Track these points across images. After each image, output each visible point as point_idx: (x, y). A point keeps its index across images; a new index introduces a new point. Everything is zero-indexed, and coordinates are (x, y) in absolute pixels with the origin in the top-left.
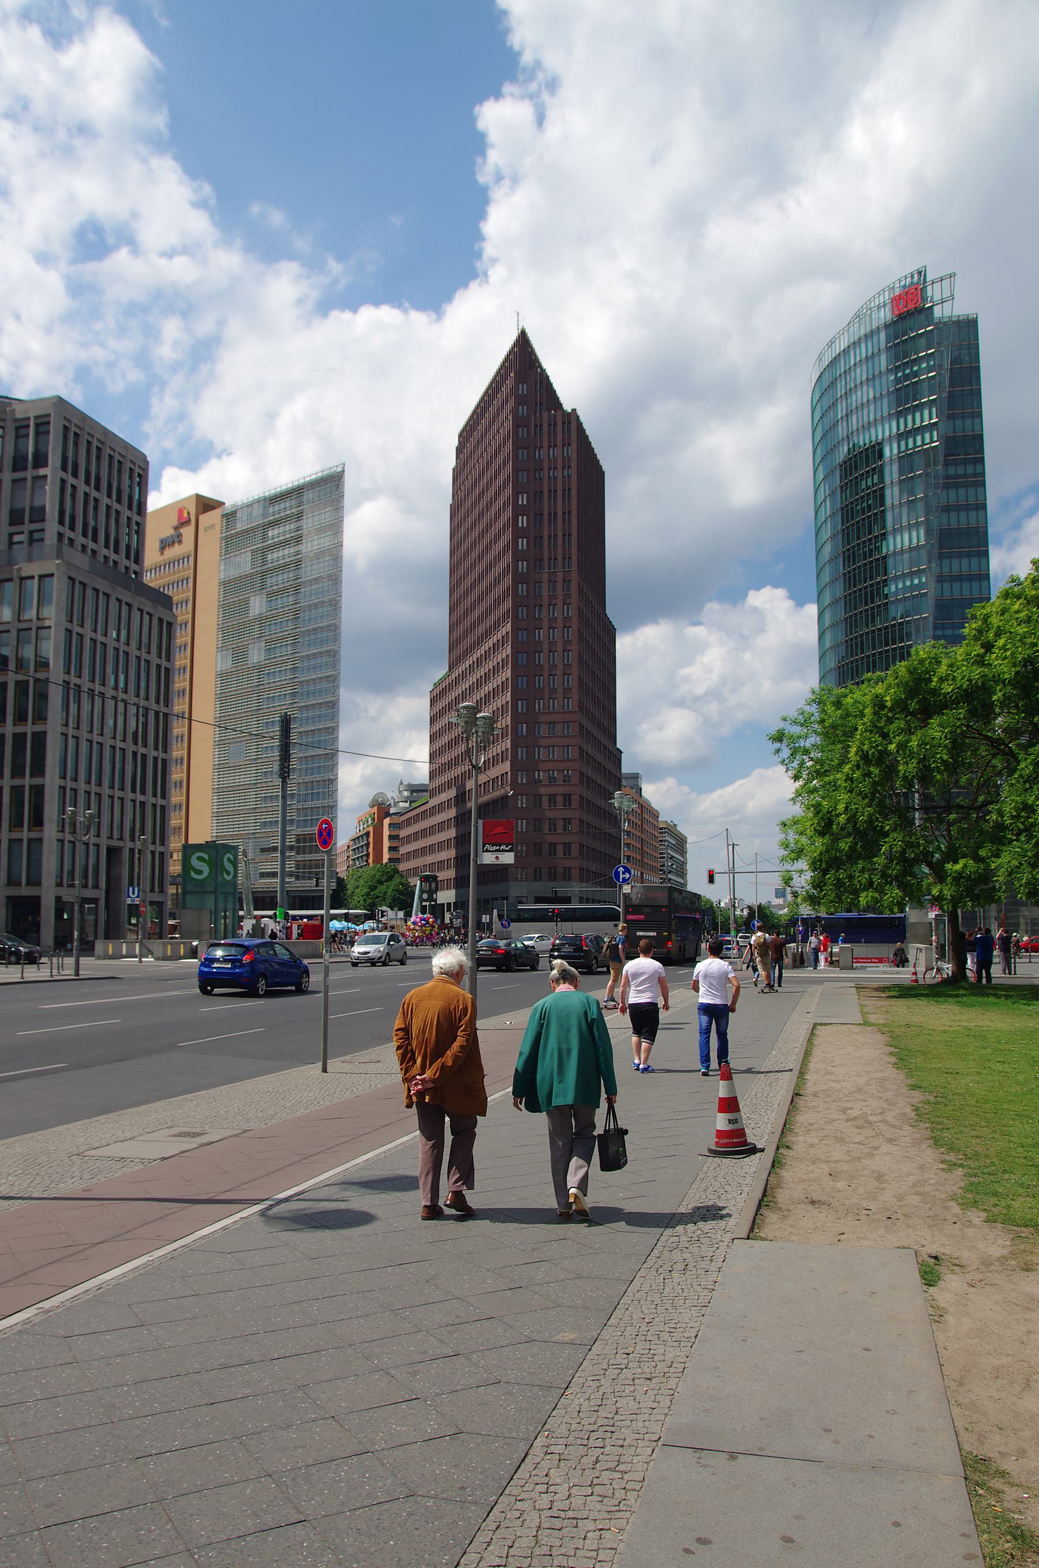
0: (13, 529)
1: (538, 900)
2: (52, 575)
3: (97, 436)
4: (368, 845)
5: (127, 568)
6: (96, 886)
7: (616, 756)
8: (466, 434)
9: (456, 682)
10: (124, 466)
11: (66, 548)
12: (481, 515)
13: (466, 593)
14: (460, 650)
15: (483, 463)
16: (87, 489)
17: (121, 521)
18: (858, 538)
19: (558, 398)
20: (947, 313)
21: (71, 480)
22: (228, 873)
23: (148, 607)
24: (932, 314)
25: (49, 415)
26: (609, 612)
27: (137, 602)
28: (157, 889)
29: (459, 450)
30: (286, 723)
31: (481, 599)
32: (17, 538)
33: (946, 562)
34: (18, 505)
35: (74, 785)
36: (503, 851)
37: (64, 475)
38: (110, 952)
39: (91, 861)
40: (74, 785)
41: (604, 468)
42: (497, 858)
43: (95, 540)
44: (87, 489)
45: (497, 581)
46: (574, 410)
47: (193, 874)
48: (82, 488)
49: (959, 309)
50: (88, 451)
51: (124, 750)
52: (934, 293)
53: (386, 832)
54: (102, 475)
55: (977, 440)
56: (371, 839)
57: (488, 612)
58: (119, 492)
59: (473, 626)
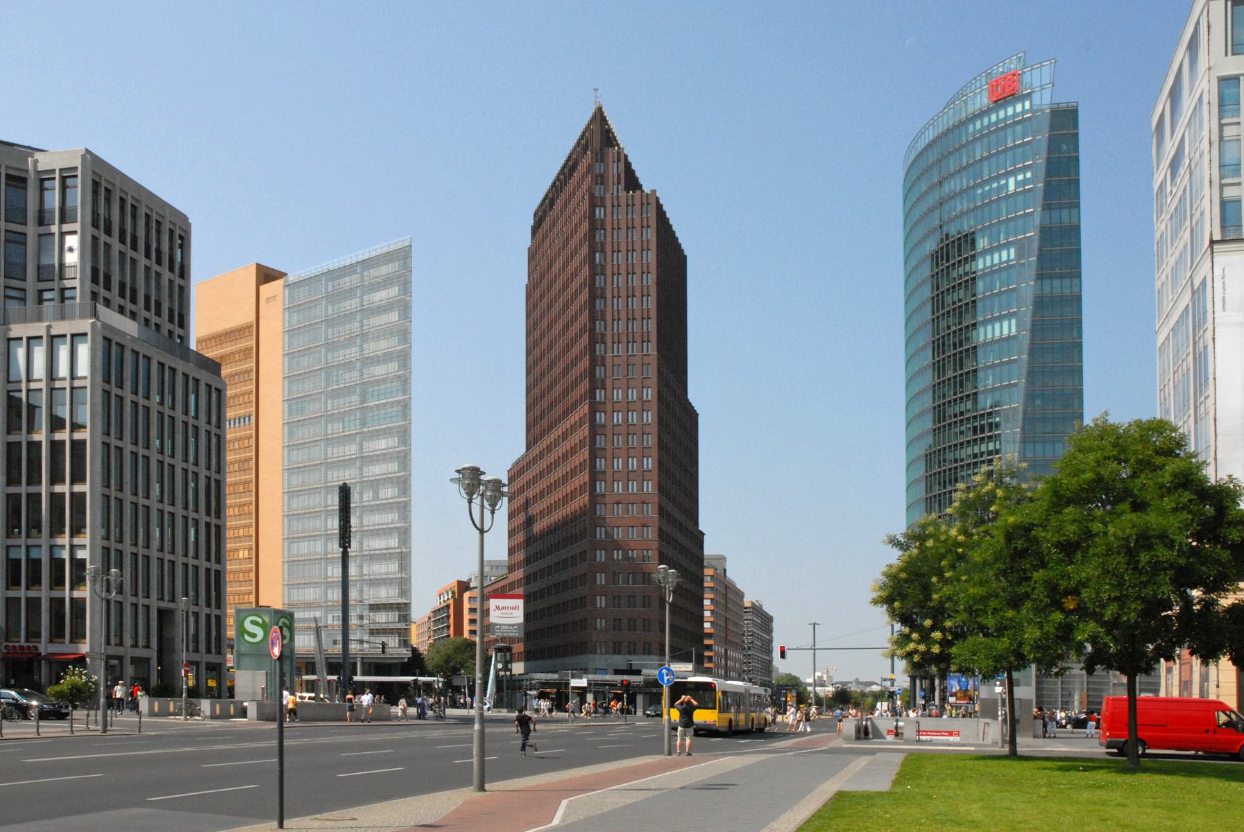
0: (42, 286)
1: (617, 672)
4: (448, 617)
5: (170, 332)
6: (148, 646)
7: (698, 538)
9: (535, 461)
10: (163, 227)
11: (101, 308)
15: (558, 243)
18: (955, 394)
19: (680, 245)
23: (194, 372)
25: (76, 168)
26: (692, 397)
27: (181, 366)
28: (213, 650)
30: (345, 492)
32: (47, 295)
33: (1047, 283)
35: (171, 557)
37: (96, 232)
38: (156, 709)
39: (192, 631)
40: (171, 557)
41: (686, 253)
46: (654, 192)
47: (247, 637)
48: (116, 246)
50: (147, 225)
53: (466, 606)
54: (138, 234)
55: (1074, 231)
56: (451, 611)
58: (159, 252)
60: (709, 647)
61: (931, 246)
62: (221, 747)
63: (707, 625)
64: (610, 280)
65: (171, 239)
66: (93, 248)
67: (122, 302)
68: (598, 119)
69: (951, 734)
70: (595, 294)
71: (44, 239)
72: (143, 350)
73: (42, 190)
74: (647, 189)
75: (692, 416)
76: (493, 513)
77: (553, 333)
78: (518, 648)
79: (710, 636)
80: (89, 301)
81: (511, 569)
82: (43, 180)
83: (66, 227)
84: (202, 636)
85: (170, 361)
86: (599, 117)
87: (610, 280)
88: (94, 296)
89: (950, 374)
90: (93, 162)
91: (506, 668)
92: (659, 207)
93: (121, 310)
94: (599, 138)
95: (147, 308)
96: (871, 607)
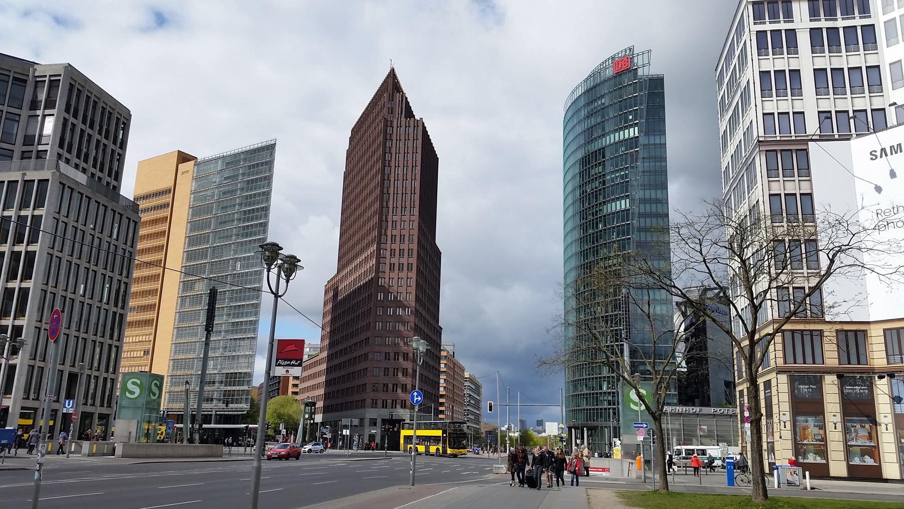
2: (48, 180)
3: (95, 93)
5: (108, 183)
8: (355, 131)
11: (62, 164)
12: (362, 179)
13: (351, 226)
14: (344, 260)
16: (99, 137)
17: (107, 150)
20: (646, 73)
21: (72, 120)
22: (154, 394)
24: (637, 73)
26: (438, 242)
28: (105, 405)
29: (351, 139)
31: (359, 229)
34: (30, 133)
36: (293, 365)
37: (67, 116)
42: (287, 371)
43: (101, 170)
44: (99, 137)
45: (369, 219)
46: (421, 119)
48: (80, 126)
49: (653, 70)
51: (91, 305)
52: (639, 61)
54: (79, 108)
57: (363, 238)
59: (353, 247)
60: (442, 404)
61: (580, 155)
62: (66, 481)
63: (441, 389)
64: (391, 154)
65: (117, 124)
66: (63, 125)
67: (77, 161)
68: (390, 81)
69: (604, 470)
70: (385, 164)
71: (32, 119)
72: (86, 192)
73: (36, 88)
74: (417, 117)
75: (438, 254)
76: (287, 282)
77: (358, 212)
78: (320, 404)
79: (442, 396)
80: (55, 158)
81: (322, 350)
82: (38, 84)
83: (47, 112)
84: (99, 394)
85: (103, 200)
86: (392, 75)
87: (391, 154)
88: (60, 156)
89: (591, 231)
90: (69, 68)
91: (311, 418)
92: (424, 128)
93: (77, 166)
94: (392, 85)
95: (94, 166)
96: (616, 48)
